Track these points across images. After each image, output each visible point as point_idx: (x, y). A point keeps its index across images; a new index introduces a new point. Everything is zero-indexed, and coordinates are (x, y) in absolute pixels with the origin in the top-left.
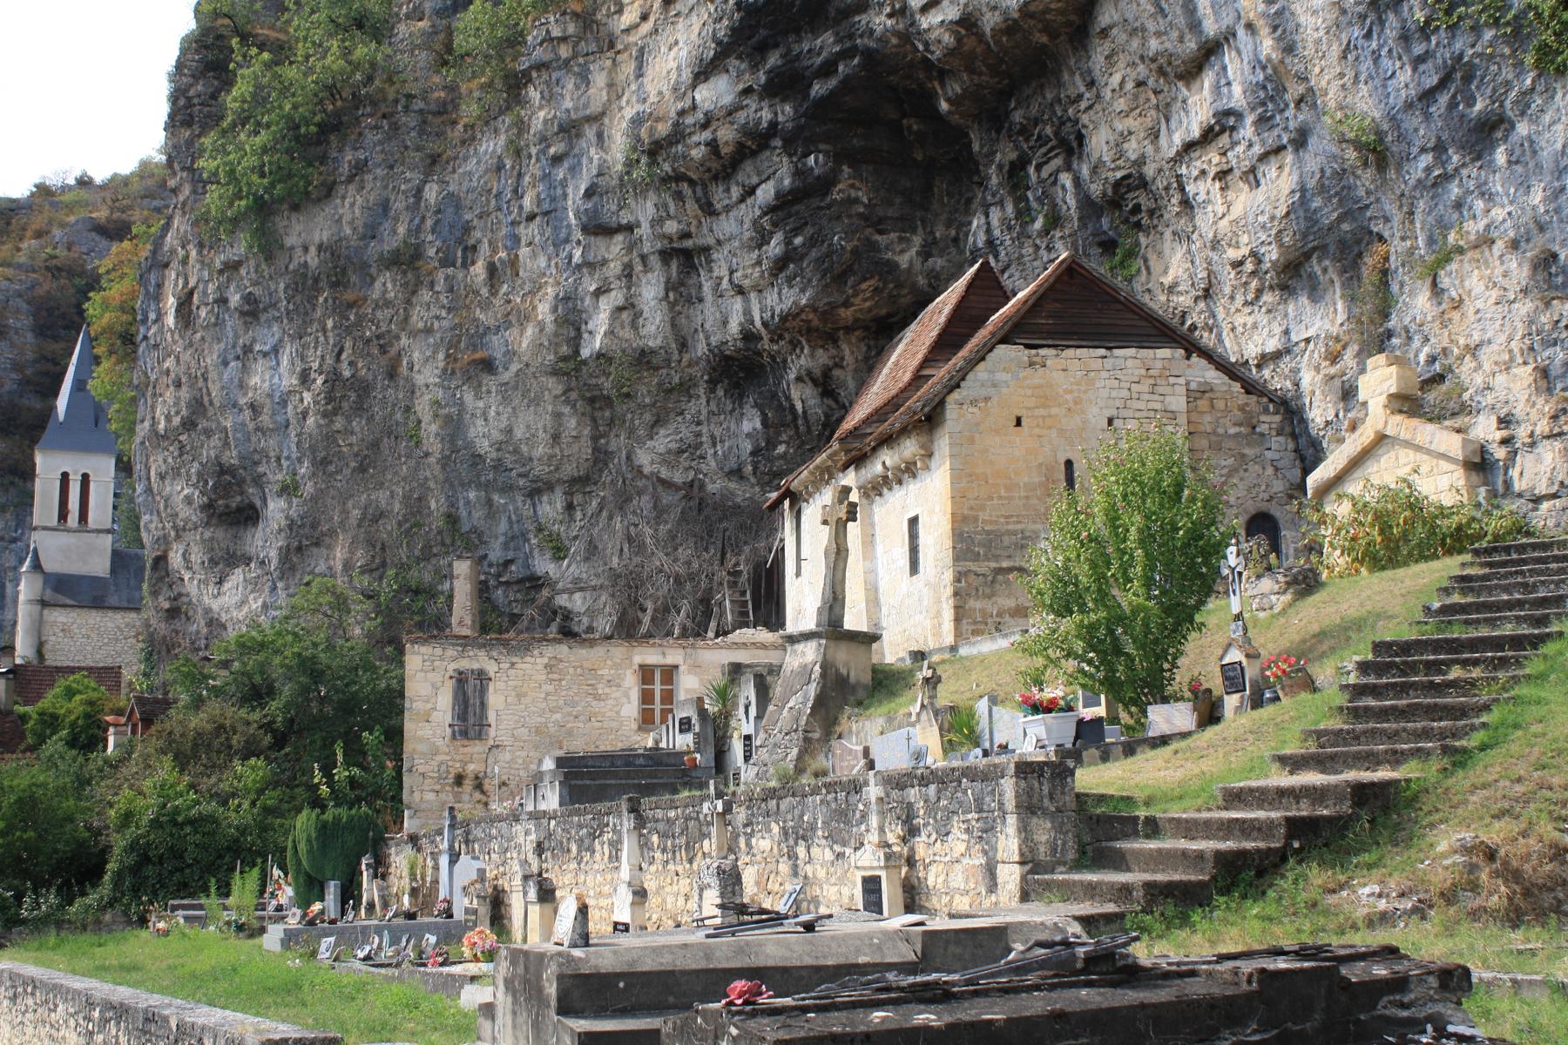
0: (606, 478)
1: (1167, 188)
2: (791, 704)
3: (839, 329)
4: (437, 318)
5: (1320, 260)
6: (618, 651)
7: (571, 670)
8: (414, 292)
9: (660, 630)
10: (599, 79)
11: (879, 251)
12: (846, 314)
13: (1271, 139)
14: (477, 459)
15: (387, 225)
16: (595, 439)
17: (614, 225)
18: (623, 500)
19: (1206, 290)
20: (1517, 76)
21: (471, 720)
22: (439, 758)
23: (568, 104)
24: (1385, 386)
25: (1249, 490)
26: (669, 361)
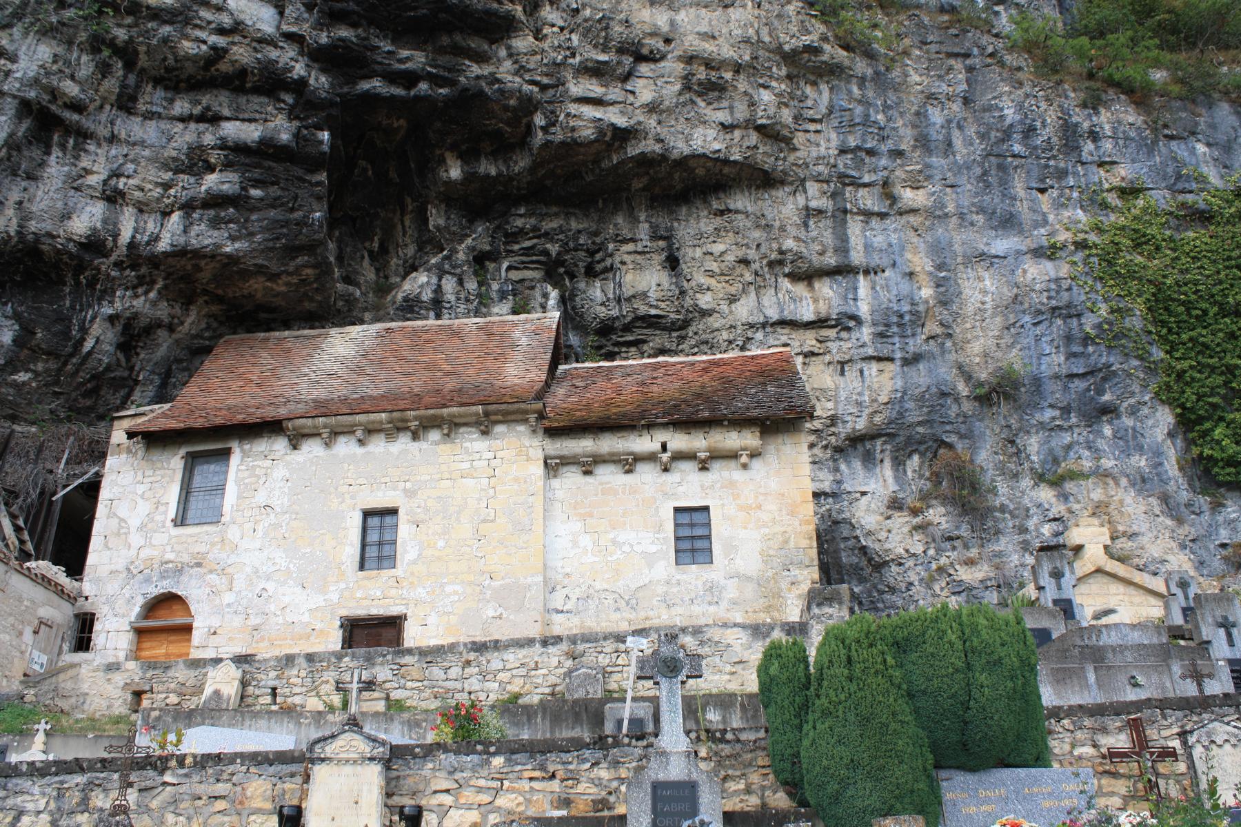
5: (885, 443)
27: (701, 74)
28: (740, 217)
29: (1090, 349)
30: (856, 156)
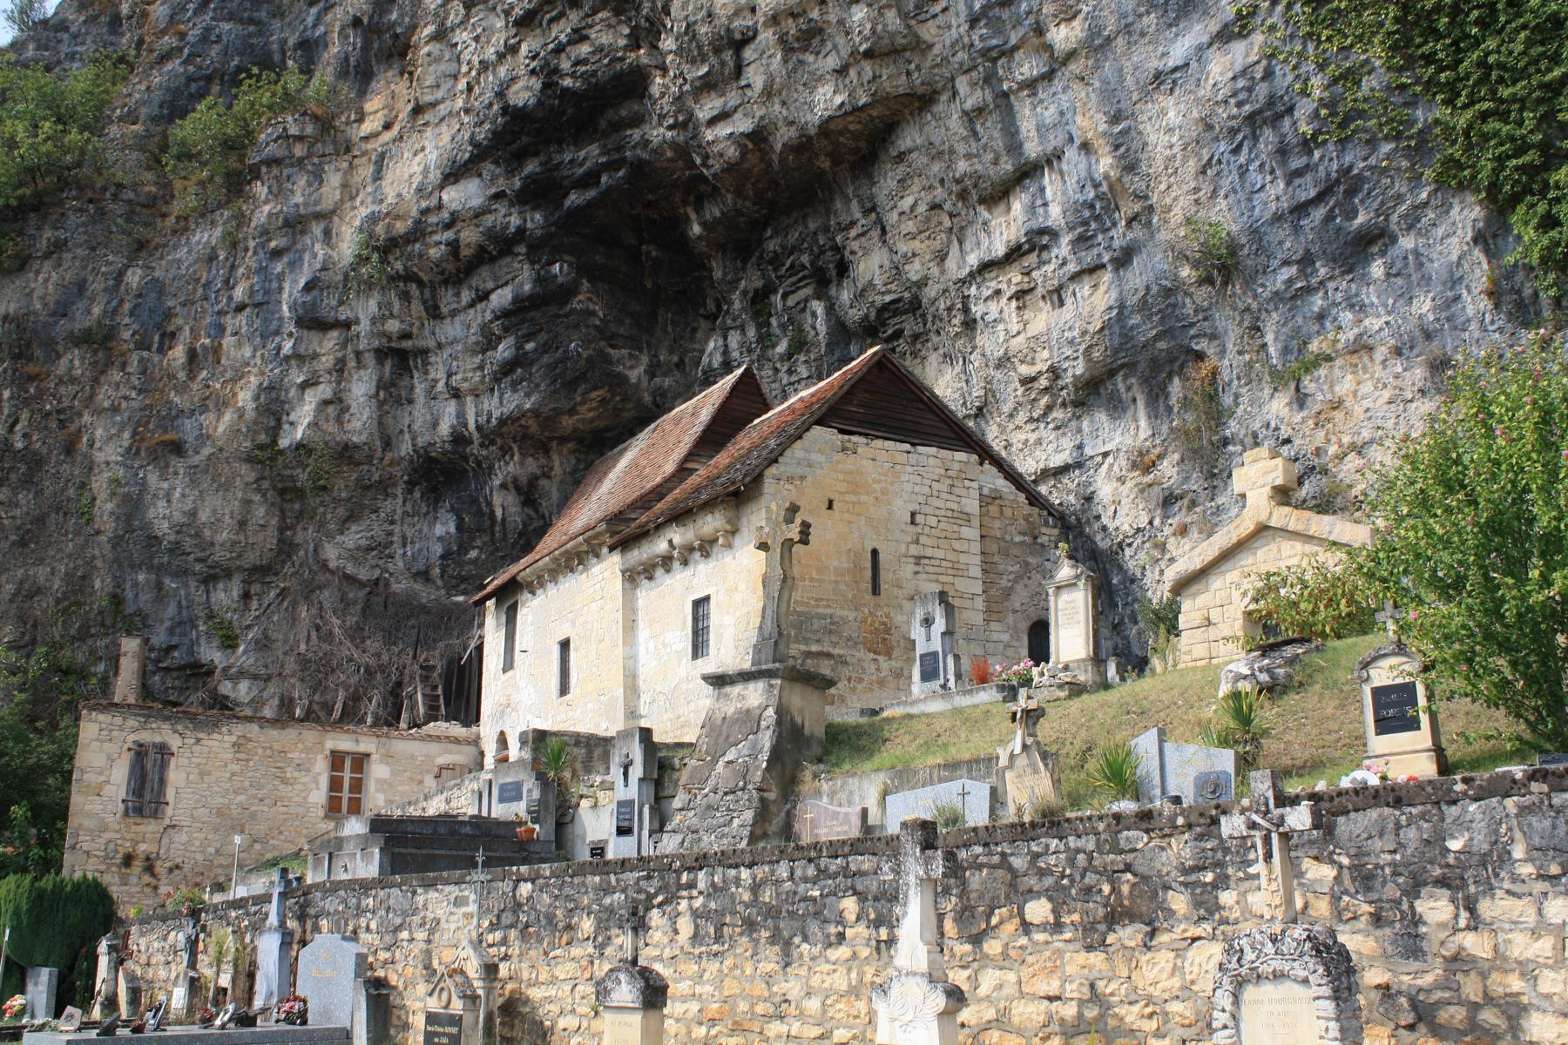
0: (288, 569)
1: (949, 309)
2: (730, 756)
3: (553, 439)
4: (126, 398)
5: (1126, 377)
6: (310, 735)
7: (260, 751)
8: (103, 372)
9: (350, 716)
10: (333, 179)
11: (611, 363)
12: (568, 422)
13: (1089, 258)
14: (153, 540)
15: (81, 305)
16: (282, 530)
17: (331, 320)
18: (309, 590)
19: (980, 409)
20: (1411, 190)
21: (148, 796)
22: (107, 836)
23: (298, 199)
24: (1270, 478)
25: (1031, 597)
26: (370, 458)
27: (791, 27)
28: (914, 155)
29: (1317, 154)
30: (989, 19)
